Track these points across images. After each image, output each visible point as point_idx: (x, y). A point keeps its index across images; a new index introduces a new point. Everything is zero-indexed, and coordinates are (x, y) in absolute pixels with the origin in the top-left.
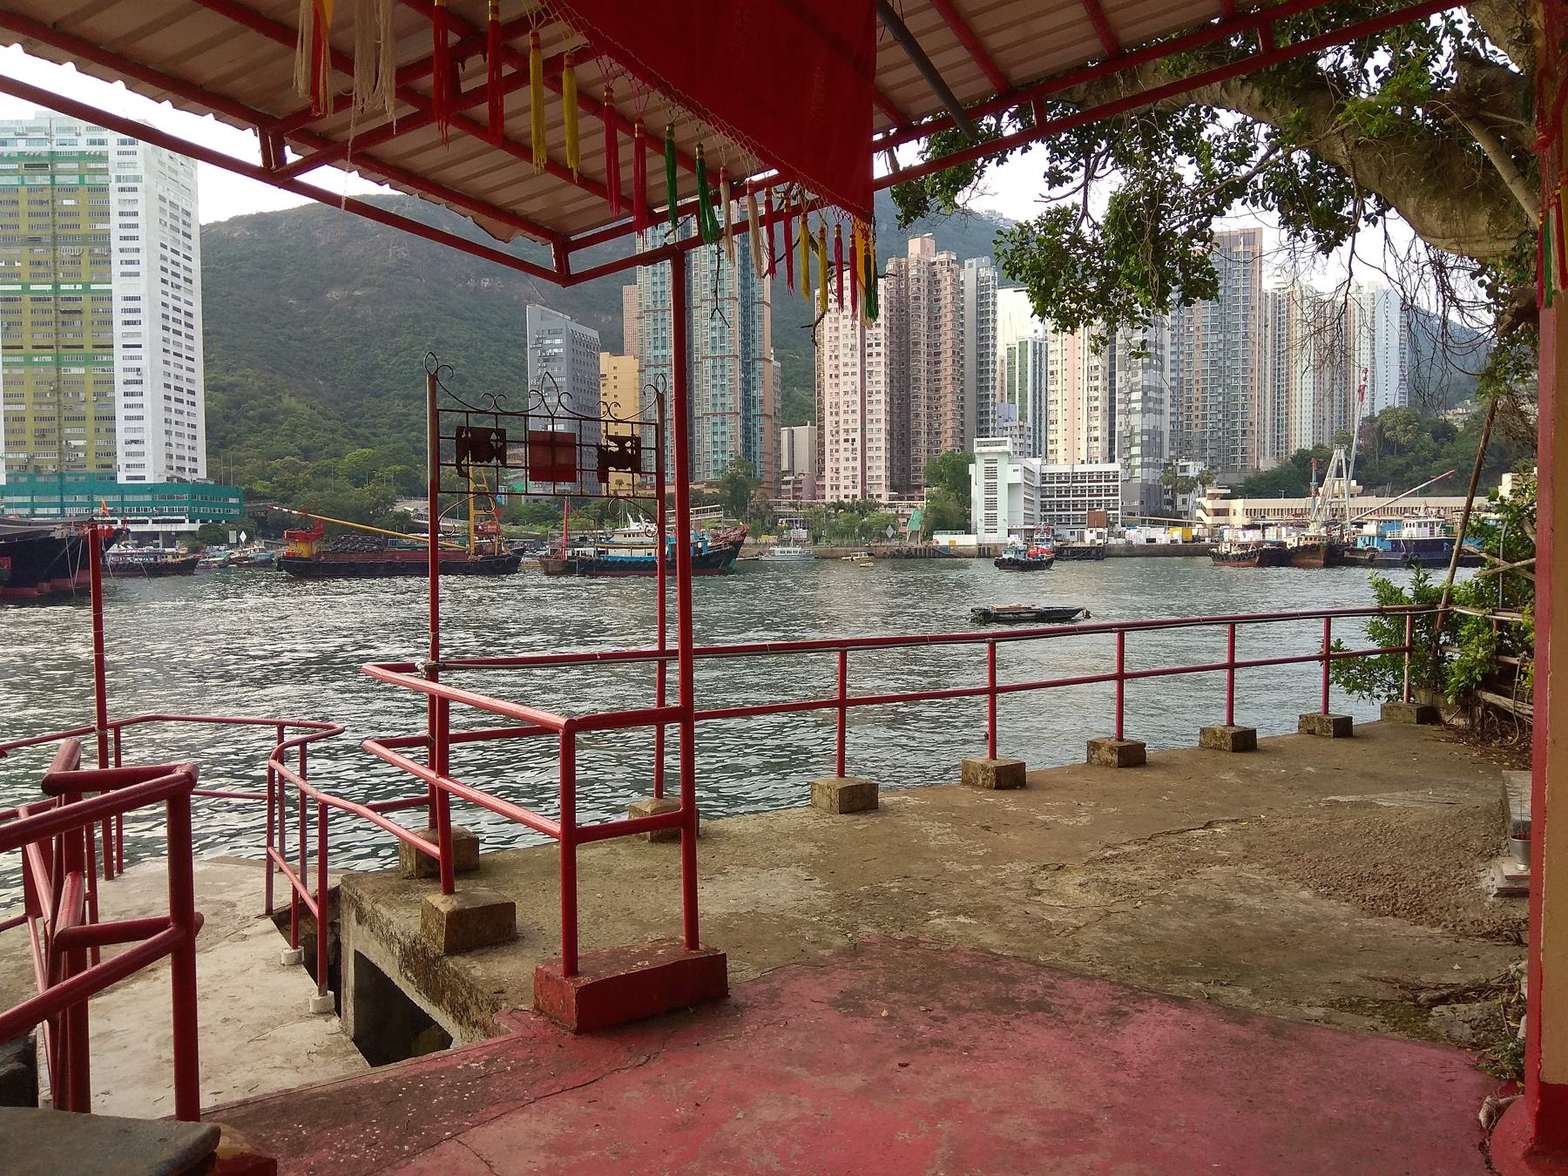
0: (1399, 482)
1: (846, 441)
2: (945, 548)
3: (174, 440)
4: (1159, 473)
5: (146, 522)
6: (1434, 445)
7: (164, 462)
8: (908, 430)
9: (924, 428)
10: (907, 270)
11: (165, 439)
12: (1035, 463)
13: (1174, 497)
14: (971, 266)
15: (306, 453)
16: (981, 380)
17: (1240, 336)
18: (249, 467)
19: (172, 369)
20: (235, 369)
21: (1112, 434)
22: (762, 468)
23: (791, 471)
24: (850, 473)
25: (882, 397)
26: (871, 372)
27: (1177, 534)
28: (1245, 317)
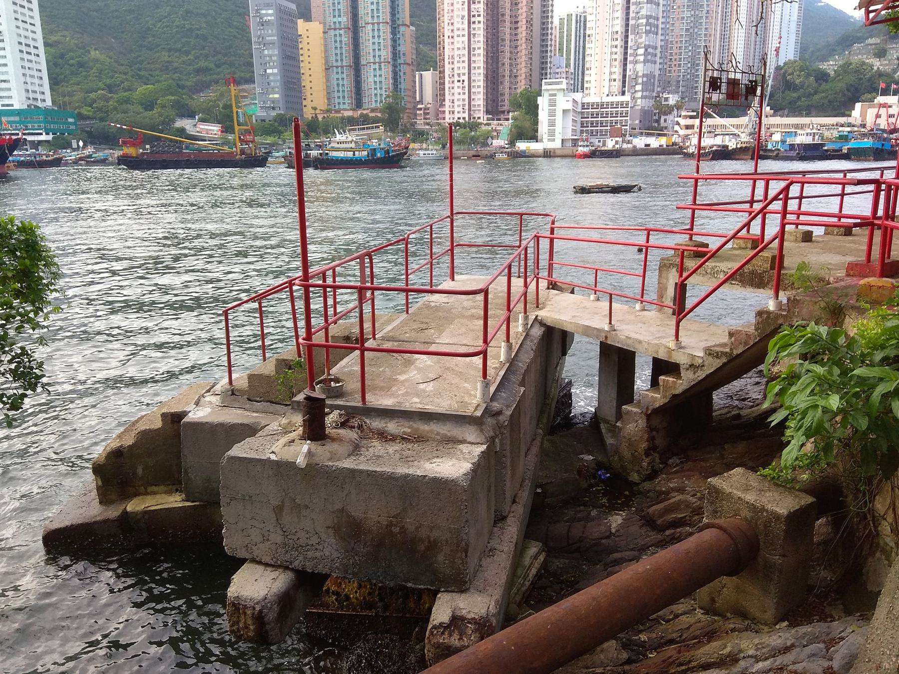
0: (794, 109)
1: (459, 81)
2: (524, 152)
3: (29, 80)
5: (41, 134)
6: (815, 85)
7: (24, 95)
9: (507, 73)
11: (23, 79)
12: (578, 96)
13: (660, 118)
15: (110, 88)
16: (543, 40)
17: (705, 12)
18: (75, 98)
19: (23, 33)
20: (57, 32)
21: (624, 76)
22: (406, 102)
23: (421, 102)
25: (481, 52)
26: (474, 35)
27: (663, 141)
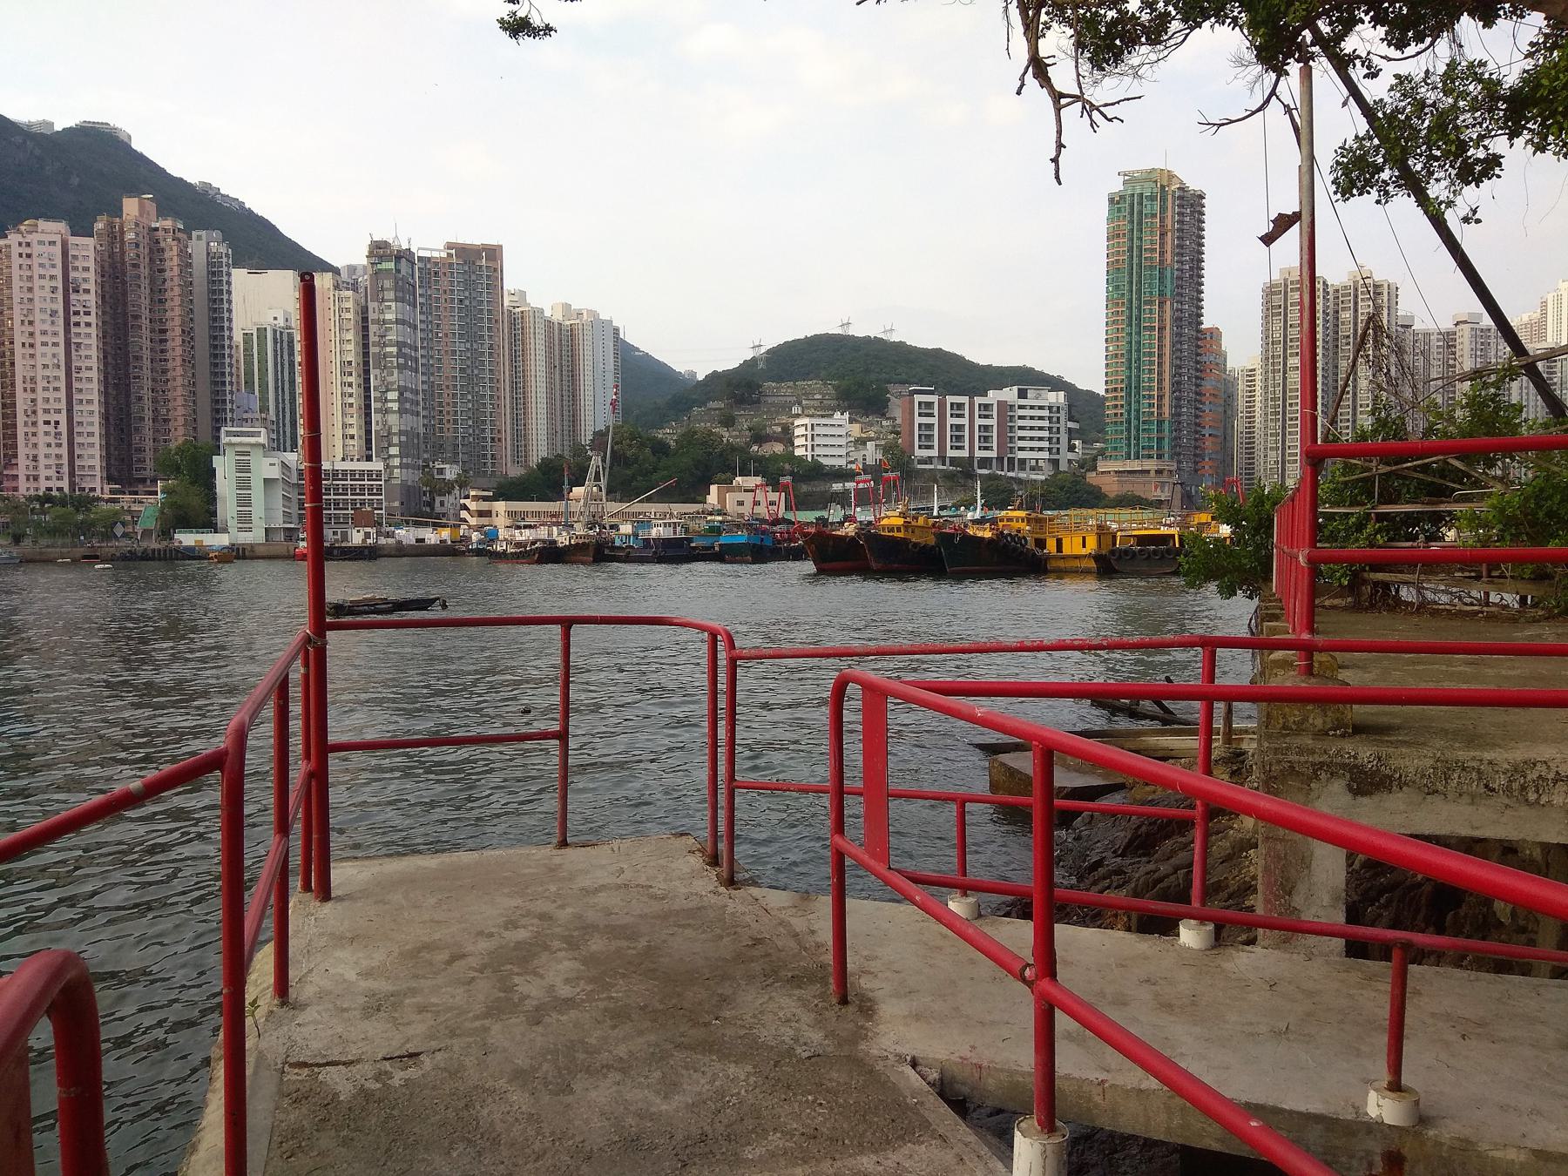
1: (47, 423)
4: (418, 475)
6: (652, 459)
8: (129, 415)
9: (148, 414)
10: (122, 233)
14: (199, 238)
16: (216, 365)
21: (368, 432)
24: (52, 461)
25: (94, 374)
27: (445, 534)
28: (490, 329)
